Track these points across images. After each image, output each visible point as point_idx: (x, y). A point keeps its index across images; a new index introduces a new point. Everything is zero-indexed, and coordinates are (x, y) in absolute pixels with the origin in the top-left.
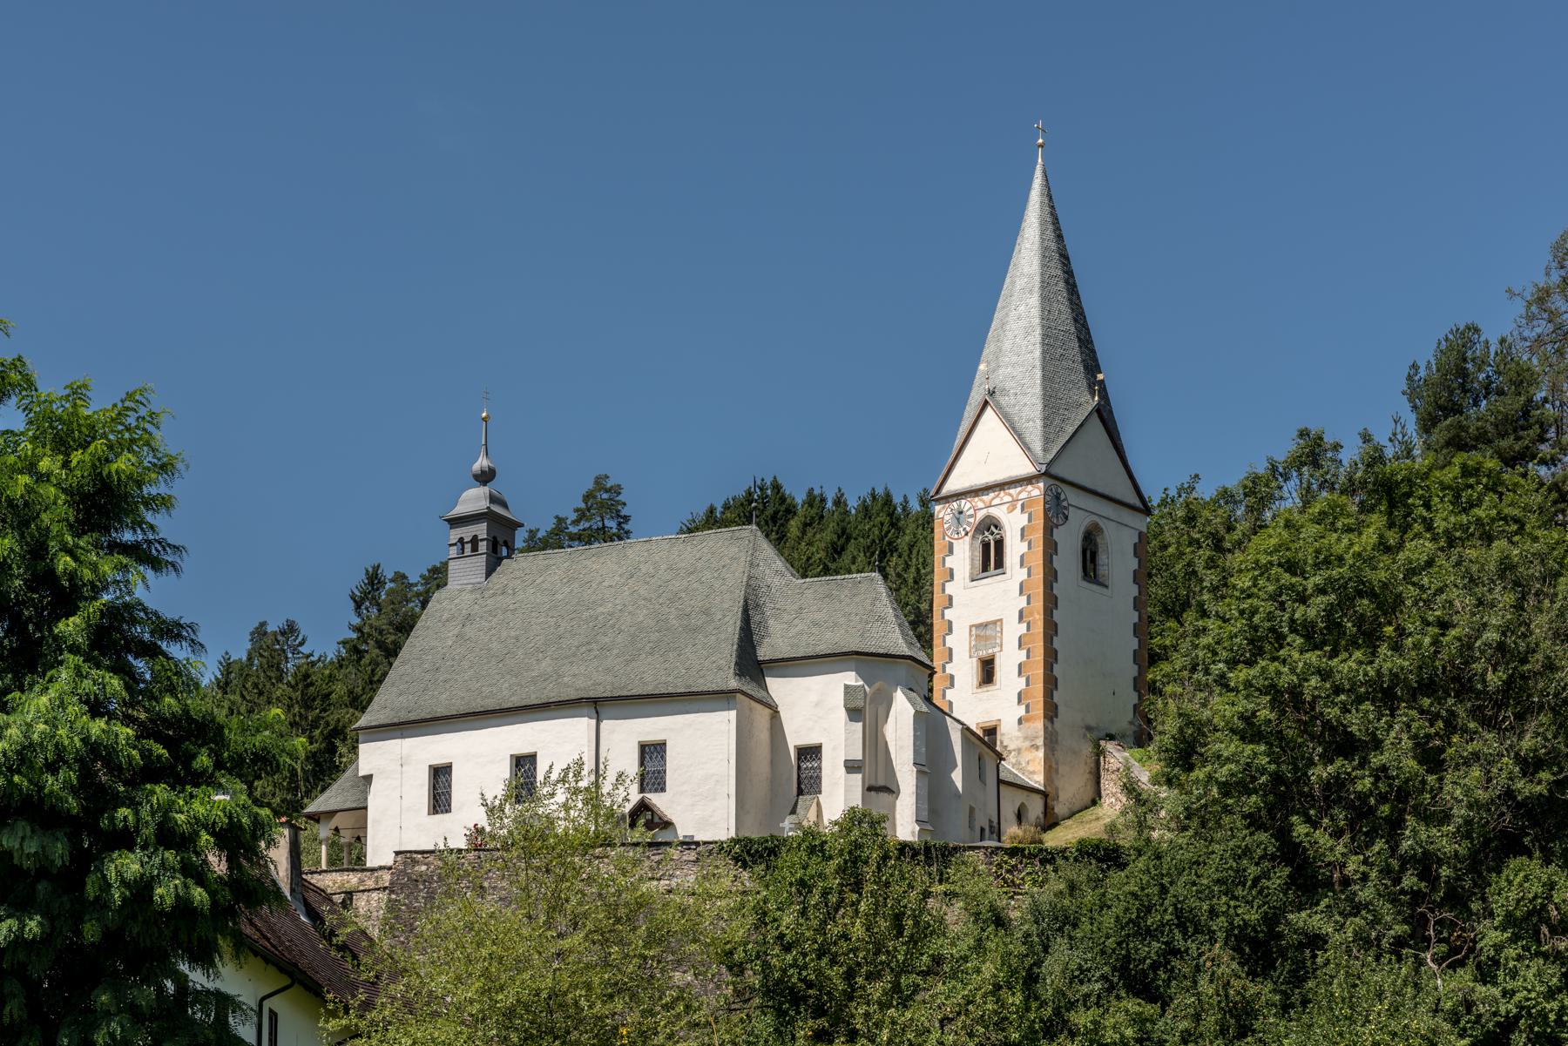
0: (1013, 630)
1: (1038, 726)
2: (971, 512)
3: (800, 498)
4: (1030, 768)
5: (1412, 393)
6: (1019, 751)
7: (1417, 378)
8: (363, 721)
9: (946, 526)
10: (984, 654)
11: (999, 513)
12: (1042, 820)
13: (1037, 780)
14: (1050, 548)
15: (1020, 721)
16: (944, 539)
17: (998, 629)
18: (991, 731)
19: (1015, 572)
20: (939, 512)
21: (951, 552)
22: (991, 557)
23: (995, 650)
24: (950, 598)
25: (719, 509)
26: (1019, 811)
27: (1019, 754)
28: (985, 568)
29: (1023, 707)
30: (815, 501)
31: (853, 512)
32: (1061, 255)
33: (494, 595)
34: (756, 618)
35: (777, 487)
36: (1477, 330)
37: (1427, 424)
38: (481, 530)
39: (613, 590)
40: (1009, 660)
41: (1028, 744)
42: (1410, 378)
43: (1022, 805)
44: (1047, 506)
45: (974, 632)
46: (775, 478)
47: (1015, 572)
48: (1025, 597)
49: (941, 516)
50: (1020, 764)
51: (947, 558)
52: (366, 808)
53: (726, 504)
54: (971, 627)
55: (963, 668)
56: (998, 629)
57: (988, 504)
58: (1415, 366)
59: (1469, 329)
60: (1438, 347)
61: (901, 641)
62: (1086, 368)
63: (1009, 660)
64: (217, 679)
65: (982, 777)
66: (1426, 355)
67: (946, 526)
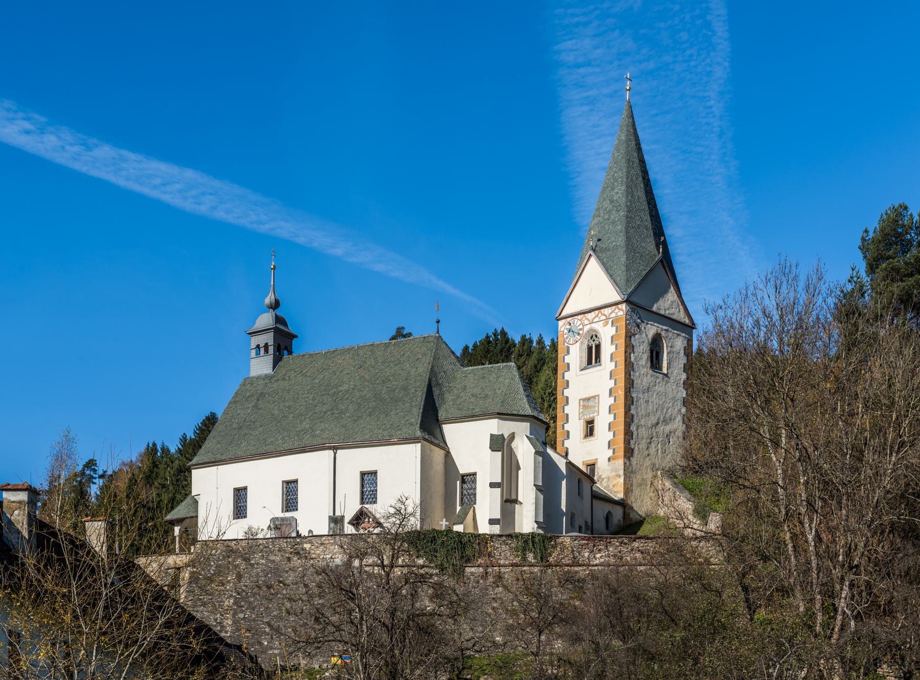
0: (606, 401)
1: (620, 463)
2: (581, 327)
3: (517, 340)
4: (615, 489)
5: (864, 248)
6: (609, 478)
7: (867, 238)
8: (193, 462)
9: (565, 336)
10: (588, 417)
11: (598, 327)
12: (622, 522)
13: (619, 495)
14: (629, 348)
15: (609, 459)
16: (564, 344)
17: (597, 401)
18: (592, 466)
19: (607, 364)
20: (562, 327)
21: (568, 353)
22: (593, 355)
23: (595, 415)
24: (568, 382)
25: (471, 347)
26: (607, 516)
27: (608, 480)
28: (589, 362)
29: (612, 450)
30: (526, 341)
31: (548, 347)
32: (640, 161)
33: (277, 381)
34: (436, 392)
35: (503, 333)
36: (906, 208)
37: (872, 268)
38: (269, 338)
39: (349, 376)
40: (603, 420)
41: (614, 474)
42: (863, 239)
43: (609, 512)
44: (628, 322)
45: (581, 404)
46: (503, 328)
47: (607, 364)
48: (613, 380)
49: (562, 330)
50: (609, 486)
51: (566, 357)
52: (197, 517)
53: (474, 344)
54: (580, 400)
55: (575, 426)
56: (597, 401)
57: (591, 322)
58: (866, 231)
59: (901, 206)
60: (881, 218)
61: (527, 406)
62: (655, 234)
63: (603, 420)
64: (179, 448)
65: (580, 493)
66: (873, 225)
67: (565, 336)
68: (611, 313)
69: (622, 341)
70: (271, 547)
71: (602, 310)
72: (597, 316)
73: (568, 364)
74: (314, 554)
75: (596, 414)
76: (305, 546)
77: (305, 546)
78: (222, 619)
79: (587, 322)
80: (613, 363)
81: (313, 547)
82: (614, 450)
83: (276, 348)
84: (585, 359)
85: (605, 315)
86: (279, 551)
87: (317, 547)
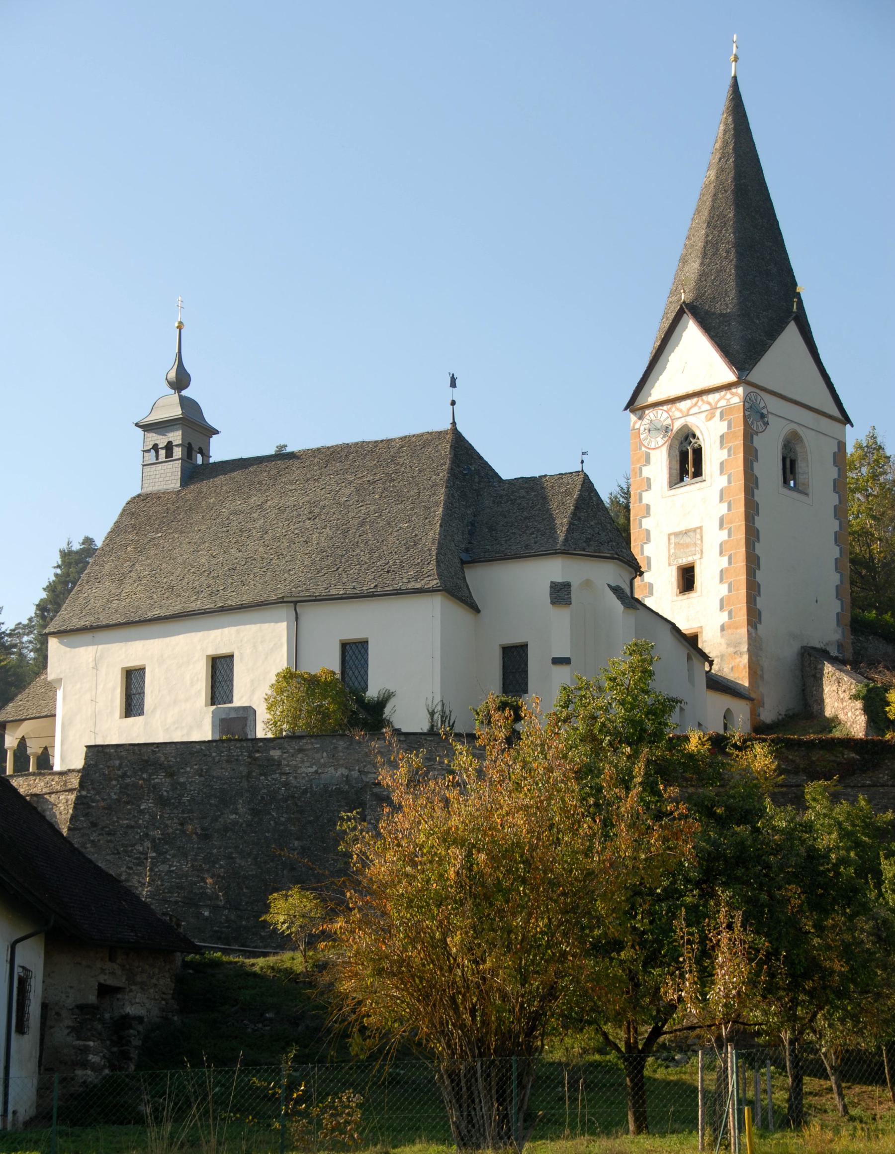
0: (715, 537)
10: (684, 561)
16: (640, 449)
17: (698, 536)
41: (731, 650)
54: (670, 535)
67: (642, 437)
68: (719, 400)
69: (739, 442)
70: (214, 754)
71: (704, 398)
72: (696, 404)
73: (649, 479)
74: (288, 765)
75: (697, 556)
76: (272, 753)
77: (272, 753)
78: (129, 874)
79: (678, 414)
80: (725, 477)
81: (285, 756)
82: (730, 613)
83: (186, 449)
84: (676, 472)
85: (709, 403)
86: (228, 761)
87: (293, 756)
